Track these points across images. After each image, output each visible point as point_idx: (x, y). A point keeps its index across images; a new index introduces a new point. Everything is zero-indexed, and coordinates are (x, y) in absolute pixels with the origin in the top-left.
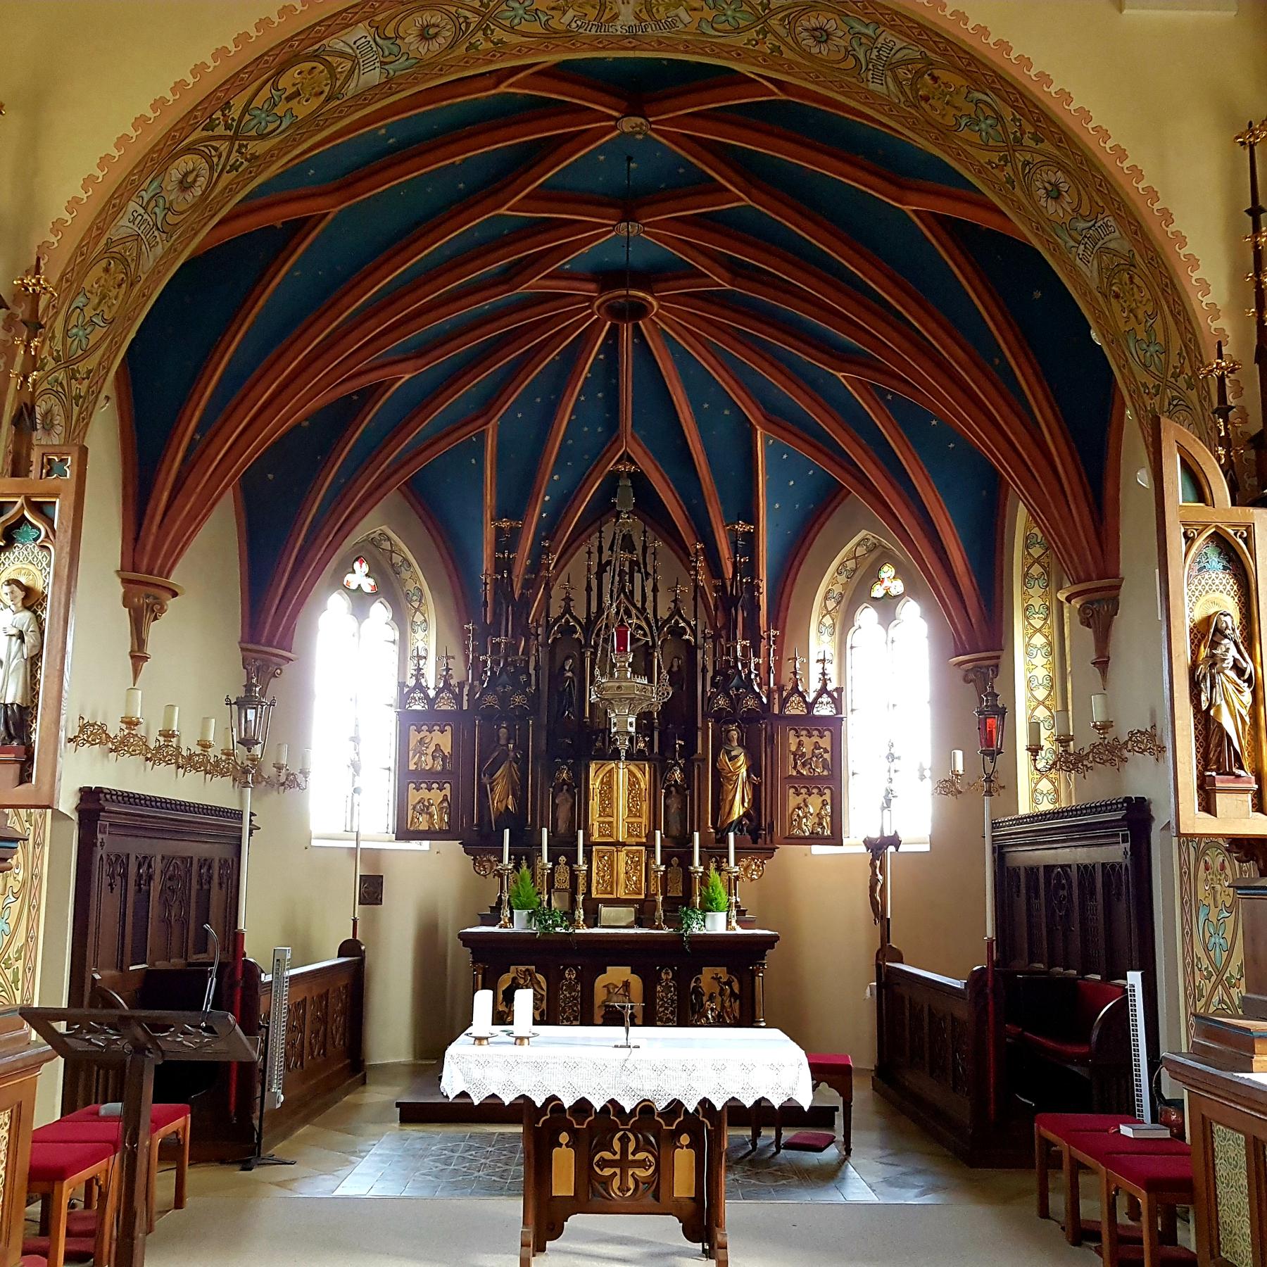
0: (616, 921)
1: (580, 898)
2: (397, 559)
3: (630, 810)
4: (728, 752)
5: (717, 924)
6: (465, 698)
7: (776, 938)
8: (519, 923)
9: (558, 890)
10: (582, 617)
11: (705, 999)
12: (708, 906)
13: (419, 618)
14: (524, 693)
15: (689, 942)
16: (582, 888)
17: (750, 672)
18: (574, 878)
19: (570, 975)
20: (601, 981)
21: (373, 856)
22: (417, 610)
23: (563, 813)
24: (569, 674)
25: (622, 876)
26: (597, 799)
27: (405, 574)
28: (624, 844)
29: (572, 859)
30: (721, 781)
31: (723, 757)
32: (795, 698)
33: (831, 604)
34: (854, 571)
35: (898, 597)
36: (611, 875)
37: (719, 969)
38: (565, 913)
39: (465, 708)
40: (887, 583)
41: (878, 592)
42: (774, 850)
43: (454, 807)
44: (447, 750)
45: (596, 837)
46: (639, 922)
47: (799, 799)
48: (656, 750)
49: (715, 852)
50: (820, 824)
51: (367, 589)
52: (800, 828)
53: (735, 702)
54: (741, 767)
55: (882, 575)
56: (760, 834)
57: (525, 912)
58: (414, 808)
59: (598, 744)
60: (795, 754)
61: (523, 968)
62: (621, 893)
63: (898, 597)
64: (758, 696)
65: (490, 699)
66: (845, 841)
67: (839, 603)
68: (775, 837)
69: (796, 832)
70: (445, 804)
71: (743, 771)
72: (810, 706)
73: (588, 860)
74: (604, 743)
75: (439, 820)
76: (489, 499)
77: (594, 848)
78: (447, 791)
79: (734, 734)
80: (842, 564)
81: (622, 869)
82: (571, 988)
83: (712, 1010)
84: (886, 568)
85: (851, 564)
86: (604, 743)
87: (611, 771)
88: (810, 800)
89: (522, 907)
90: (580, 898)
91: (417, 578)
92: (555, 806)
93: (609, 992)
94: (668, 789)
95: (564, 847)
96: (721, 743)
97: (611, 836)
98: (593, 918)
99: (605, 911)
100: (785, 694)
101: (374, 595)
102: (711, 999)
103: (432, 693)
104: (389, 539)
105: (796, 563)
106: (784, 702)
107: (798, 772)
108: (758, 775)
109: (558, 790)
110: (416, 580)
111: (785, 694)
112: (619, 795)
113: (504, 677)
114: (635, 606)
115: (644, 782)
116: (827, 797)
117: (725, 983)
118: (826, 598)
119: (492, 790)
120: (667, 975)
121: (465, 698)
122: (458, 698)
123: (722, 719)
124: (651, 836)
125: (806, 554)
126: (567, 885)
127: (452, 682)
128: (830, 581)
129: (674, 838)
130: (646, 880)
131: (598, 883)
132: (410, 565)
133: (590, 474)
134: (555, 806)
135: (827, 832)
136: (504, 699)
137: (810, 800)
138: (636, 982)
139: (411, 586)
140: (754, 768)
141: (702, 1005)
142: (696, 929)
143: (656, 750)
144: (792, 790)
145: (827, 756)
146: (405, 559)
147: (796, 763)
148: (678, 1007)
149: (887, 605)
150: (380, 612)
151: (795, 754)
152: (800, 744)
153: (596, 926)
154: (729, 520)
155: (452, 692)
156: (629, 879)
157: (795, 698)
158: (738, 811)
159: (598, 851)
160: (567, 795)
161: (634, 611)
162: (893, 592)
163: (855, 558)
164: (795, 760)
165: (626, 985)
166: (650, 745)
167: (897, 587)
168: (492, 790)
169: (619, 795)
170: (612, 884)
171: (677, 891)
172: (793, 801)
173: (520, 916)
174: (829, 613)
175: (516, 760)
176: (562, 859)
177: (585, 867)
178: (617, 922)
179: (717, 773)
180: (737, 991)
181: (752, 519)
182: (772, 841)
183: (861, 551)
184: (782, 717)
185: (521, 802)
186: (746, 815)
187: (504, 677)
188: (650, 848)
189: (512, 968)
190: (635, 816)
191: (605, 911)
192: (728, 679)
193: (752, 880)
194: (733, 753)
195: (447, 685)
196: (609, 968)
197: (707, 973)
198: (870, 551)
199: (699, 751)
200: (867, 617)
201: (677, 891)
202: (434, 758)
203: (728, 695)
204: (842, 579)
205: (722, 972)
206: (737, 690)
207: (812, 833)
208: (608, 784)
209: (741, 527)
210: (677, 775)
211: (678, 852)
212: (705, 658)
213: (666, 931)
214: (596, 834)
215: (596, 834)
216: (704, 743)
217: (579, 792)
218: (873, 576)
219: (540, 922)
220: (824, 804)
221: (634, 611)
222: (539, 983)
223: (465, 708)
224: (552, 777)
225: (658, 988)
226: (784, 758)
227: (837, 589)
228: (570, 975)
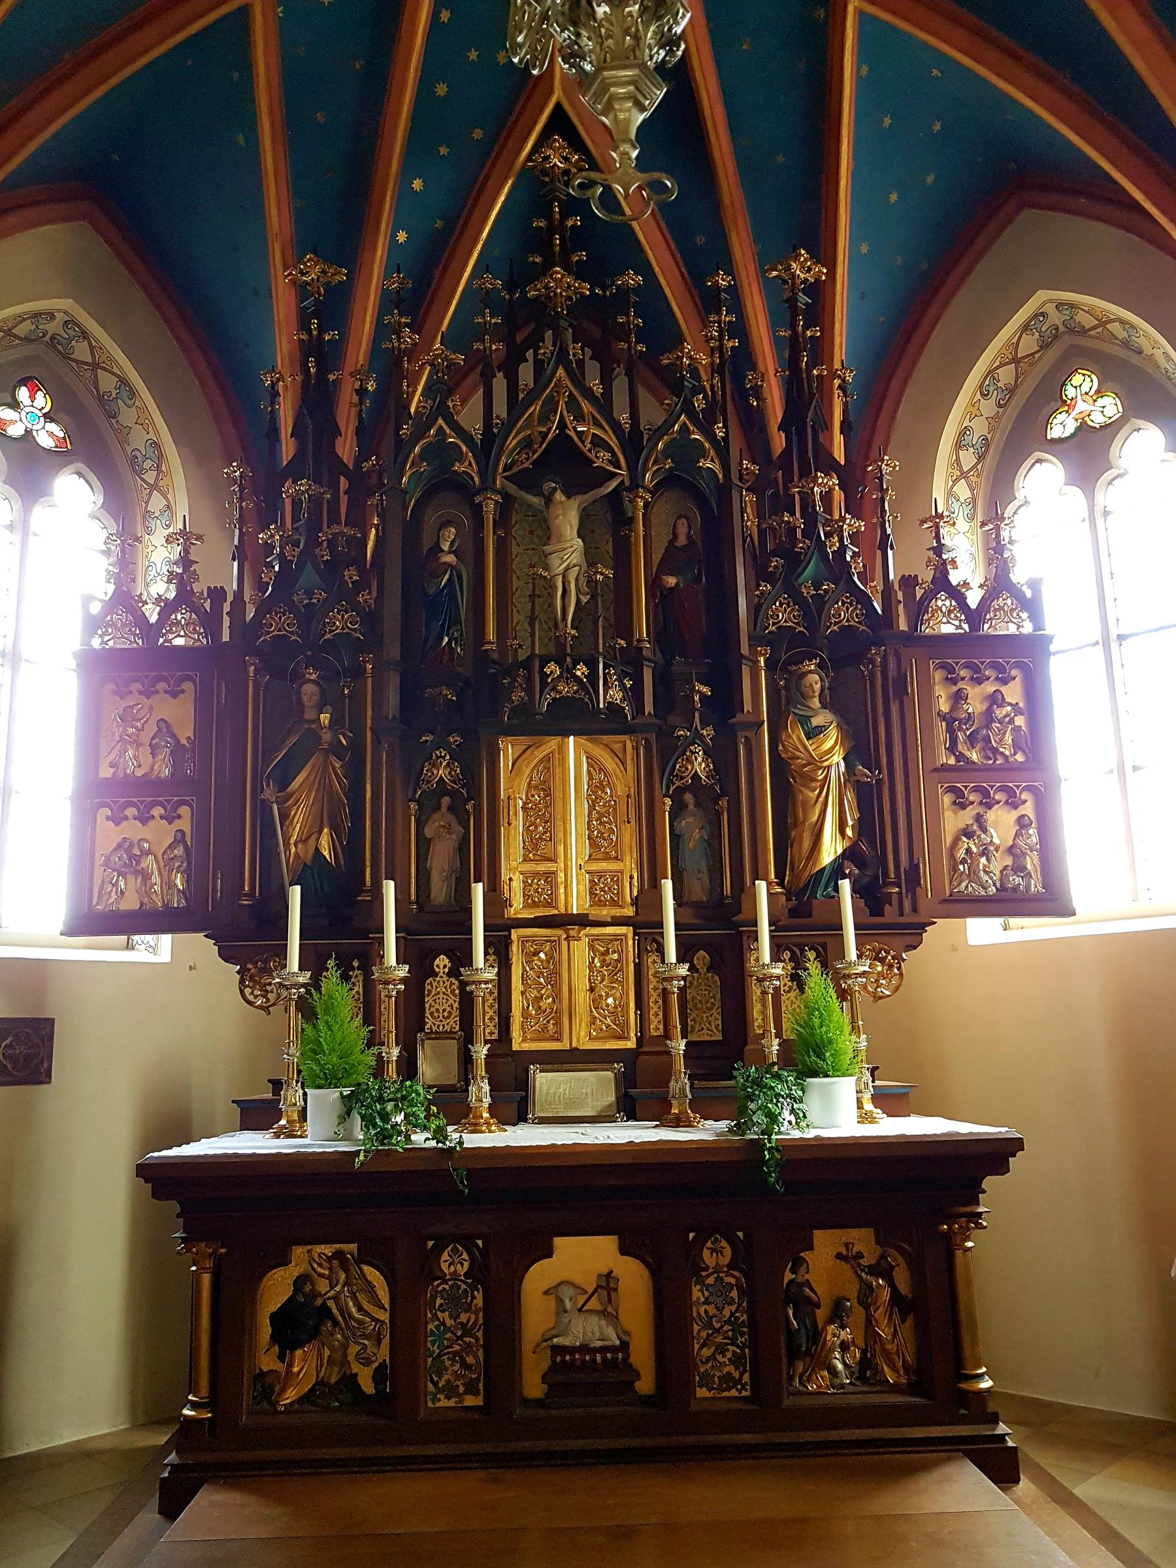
0: (571, 1103)
1: (481, 1051)
2: (107, 382)
3: (593, 844)
4: (804, 721)
5: (836, 1112)
6: (226, 620)
7: (1015, 1145)
8: (318, 1129)
9: (437, 1036)
10: (476, 428)
11: (821, 1314)
12: (808, 1059)
13: (157, 503)
14: (355, 606)
15: (778, 1163)
16: (485, 1026)
17: (843, 549)
18: (467, 1002)
19: (454, 1264)
20: (539, 1277)
21: (34, 974)
22: (154, 487)
23: (441, 858)
24: (450, 559)
25: (582, 999)
26: (519, 823)
27: (127, 416)
28: (583, 921)
29: (462, 957)
30: (789, 780)
31: (795, 735)
32: (943, 602)
33: (968, 459)
34: (1012, 390)
35: (1111, 429)
36: (557, 997)
37: (853, 1234)
38: (441, 1089)
39: (226, 638)
40: (1081, 406)
41: (1062, 426)
42: (923, 926)
43: (204, 856)
44: (186, 732)
45: (517, 908)
46: (629, 1107)
47: (966, 817)
48: (649, 708)
49: (806, 928)
50: (1018, 868)
51: (45, 441)
52: (973, 875)
53: (813, 611)
54: (831, 751)
55: (1070, 392)
56: (897, 894)
57: (333, 1094)
58: (106, 864)
59: (518, 696)
60: (949, 719)
61: (328, 1250)
62: (581, 1038)
63: (1111, 429)
64: (864, 600)
65: (281, 624)
66: (1077, 902)
67: (981, 458)
68: (922, 904)
69: (974, 889)
70: (179, 851)
71: (837, 758)
72: (975, 617)
73: (499, 948)
74: (529, 689)
75: (170, 885)
76: (277, 213)
77: (514, 934)
78: (185, 824)
79: (814, 681)
80: (991, 373)
81: (581, 980)
82: (456, 1303)
83: (844, 1347)
84: (1077, 379)
85: (1006, 375)
86: (529, 689)
87: (547, 759)
88: (991, 816)
89: (328, 1080)
90: (481, 1051)
91: (149, 422)
92: (424, 845)
93: (561, 1310)
94: (678, 799)
95: (436, 932)
96: (786, 700)
97: (549, 905)
98: (515, 1105)
99: (545, 1082)
100: (919, 593)
101: (60, 457)
102: (838, 1314)
103: (152, 614)
104: (85, 335)
105: (894, 384)
106: (919, 610)
107: (960, 757)
108: (872, 764)
109: (427, 807)
110: (145, 423)
111: (919, 593)
112: (568, 823)
113: (309, 570)
114: (588, 393)
115: (623, 781)
116: (1028, 809)
117: (874, 1270)
118: (959, 445)
119: (284, 817)
120: (716, 1256)
121: (226, 620)
122: (210, 622)
123: (787, 652)
124: (648, 899)
125: (914, 365)
126: (453, 1023)
127: (197, 588)
128: (967, 412)
129: (697, 905)
130: (639, 1005)
131: (525, 1014)
132: (133, 393)
133: (487, 177)
134: (424, 845)
135: (1036, 886)
136: (308, 617)
137: (991, 816)
138: (633, 1276)
139: (138, 440)
140: (859, 751)
141: (816, 1335)
142: (789, 1131)
143: (649, 708)
144: (947, 799)
145: (1020, 721)
146: (123, 381)
147: (954, 741)
148: (753, 1344)
149: (1089, 453)
150: (74, 494)
151: (949, 719)
152: (958, 698)
153: (521, 1117)
154: (773, 252)
155: (194, 609)
156: (597, 1003)
157: (943, 602)
158: (831, 849)
159: (524, 941)
160: (451, 818)
161: (586, 406)
162: (1098, 419)
163: (1016, 361)
164: (950, 730)
165: (608, 1283)
166: (635, 695)
167: (1110, 407)
168: (284, 817)
169: (568, 823)
170: (556, 1018)
171: (711, 1029)
172: (953, 821)
173: (323, 1103)
174: (964, 475)
175: (336, 750)
176: (442, 962)
177: (491, 974)
178: (574, 1119)
179: (780, 766)
180: (904, 1287)
181: (824, 254)
182: (915, 910)
183: (1029, 344)
184: (913, 638)
185: (351, 845)
186: (849, 854)
187: (309, 570)
188: (647, 927)
189: (298, 1251)
190: (607, 858)
191: (545, 1082)
192: (795, 562)
193: (877, 998)
194: (816, 721)
195: (185, 597)
196: (558, 1241)
197: (825, 1245)
198: (1044, 346)
199: (747, 707)
200: (1042, 482)
201: (711, 1029)
202: (154, 750)
203: (795, 596)
204: (988, 407)
205: (862, 1240)
206: (817, 585)
207: (1002, 889)
208: (546, 791)
209: (802, 268)
210: (699, 765)
211: (717, 932)
212: (747, 515)
213: (707, 1131)
214: (517, 902)
215: (517, 902)
216: (756, 691)
217: (478, 809)
218: (1050, 396)
219: (368, 1121)
220: (1022, 823)
221: (586, 406)
222: (370, 1288)
223: (226, 638)
224: (413, 777)
225: (696, 1293)
226: (928, 729)
227: (980, 428)
228: (454, 1264)
